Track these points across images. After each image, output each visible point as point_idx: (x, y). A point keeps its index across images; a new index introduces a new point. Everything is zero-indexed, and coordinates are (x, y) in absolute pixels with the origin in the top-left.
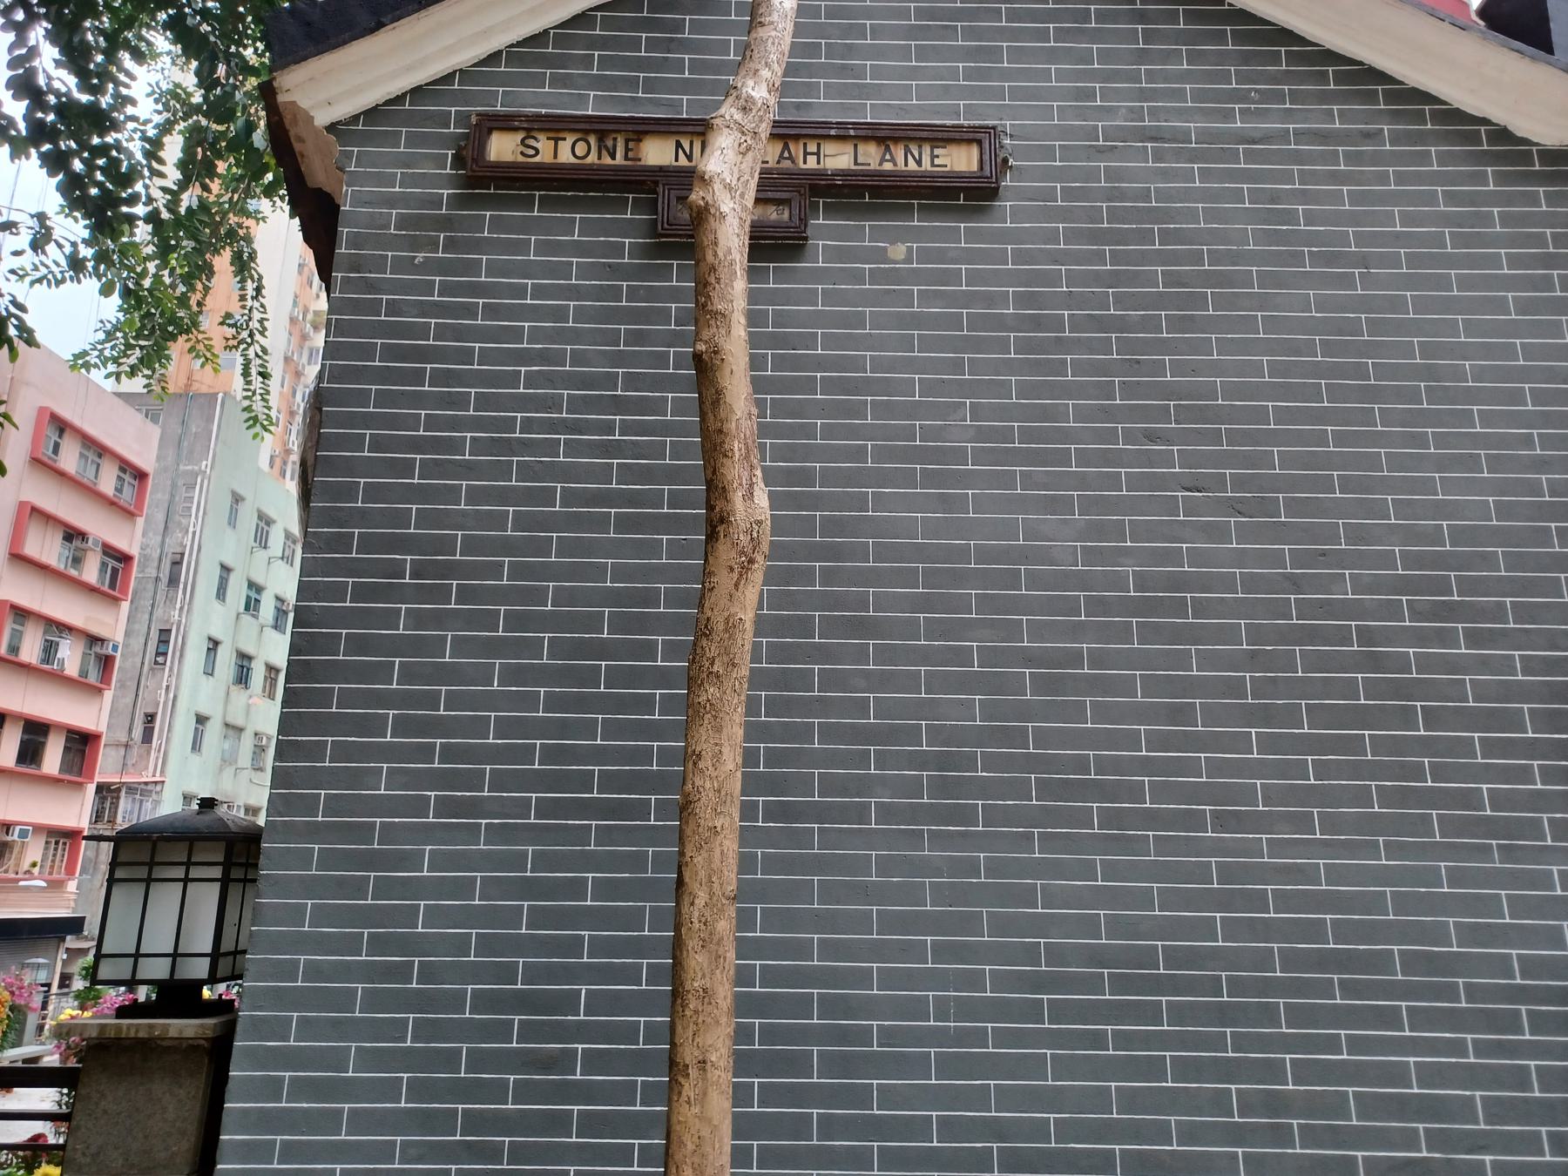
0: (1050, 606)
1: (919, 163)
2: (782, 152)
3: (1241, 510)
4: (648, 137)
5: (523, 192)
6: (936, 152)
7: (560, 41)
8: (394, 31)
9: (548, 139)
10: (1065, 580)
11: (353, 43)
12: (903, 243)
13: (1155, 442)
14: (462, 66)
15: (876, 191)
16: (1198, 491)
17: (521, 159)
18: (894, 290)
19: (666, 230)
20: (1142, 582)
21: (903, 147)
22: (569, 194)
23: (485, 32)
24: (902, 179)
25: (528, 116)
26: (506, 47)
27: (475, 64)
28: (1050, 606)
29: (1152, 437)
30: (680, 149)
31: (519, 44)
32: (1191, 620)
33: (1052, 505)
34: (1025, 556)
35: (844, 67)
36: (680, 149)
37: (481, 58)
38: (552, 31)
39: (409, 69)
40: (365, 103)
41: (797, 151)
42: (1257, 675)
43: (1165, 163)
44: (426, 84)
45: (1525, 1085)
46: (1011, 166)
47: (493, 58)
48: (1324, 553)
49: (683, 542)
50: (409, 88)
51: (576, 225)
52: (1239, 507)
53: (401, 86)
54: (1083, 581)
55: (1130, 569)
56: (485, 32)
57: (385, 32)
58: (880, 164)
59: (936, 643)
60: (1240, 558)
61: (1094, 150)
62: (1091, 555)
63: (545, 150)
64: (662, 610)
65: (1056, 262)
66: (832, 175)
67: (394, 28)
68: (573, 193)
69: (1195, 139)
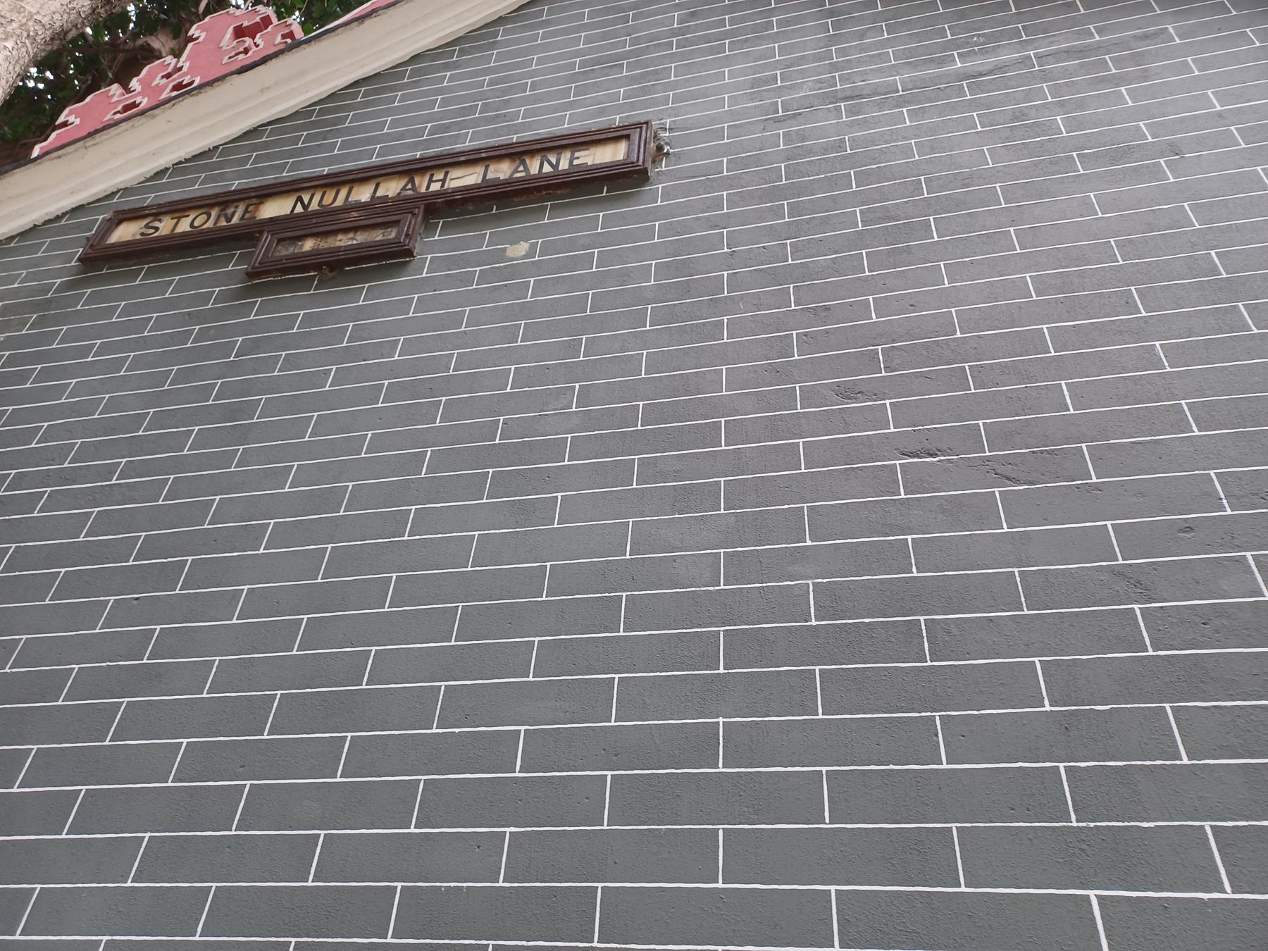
0: (663, 654)
2: (406, 185)
3: (1011, 475)
4: (269, 199)
6: (577, 155)
8: (59, 160)
9: (172, 219)
10: (697, 609)
11: (14, 171)
12: (526, 241)
13: (855, 398)
16: (931, 455)
18: (505, 285)
20: (831, 602)
21: (540, 158)
22: (178, 261)
23: (154, 154)
26: (173, 165)
28: (663, 654)
29: (847, 393)
30: (299, 203)
32: (929, 663)
33: (682, 499)
34: (630, 576)
35: (497, 116)
36: (299, 203)
42: (1083, 765)
43: (862, 115)
45: (1038, 57)
48: (1188, 528)
49: (135, 602)
50: (70, 208)
51: (172, 286)
52: (1007, 470)
54: (726, 609)
55: (810, 582)
56: (154, 154)
57: (49, 160)
59: (457, 730)
60: (1019, 548)
61: (772, 122)
62: (739, 567)
63: (165, 226)
64: (720, 885)
65: (716, 227)
66: (451, 193)
69: (902, 87)
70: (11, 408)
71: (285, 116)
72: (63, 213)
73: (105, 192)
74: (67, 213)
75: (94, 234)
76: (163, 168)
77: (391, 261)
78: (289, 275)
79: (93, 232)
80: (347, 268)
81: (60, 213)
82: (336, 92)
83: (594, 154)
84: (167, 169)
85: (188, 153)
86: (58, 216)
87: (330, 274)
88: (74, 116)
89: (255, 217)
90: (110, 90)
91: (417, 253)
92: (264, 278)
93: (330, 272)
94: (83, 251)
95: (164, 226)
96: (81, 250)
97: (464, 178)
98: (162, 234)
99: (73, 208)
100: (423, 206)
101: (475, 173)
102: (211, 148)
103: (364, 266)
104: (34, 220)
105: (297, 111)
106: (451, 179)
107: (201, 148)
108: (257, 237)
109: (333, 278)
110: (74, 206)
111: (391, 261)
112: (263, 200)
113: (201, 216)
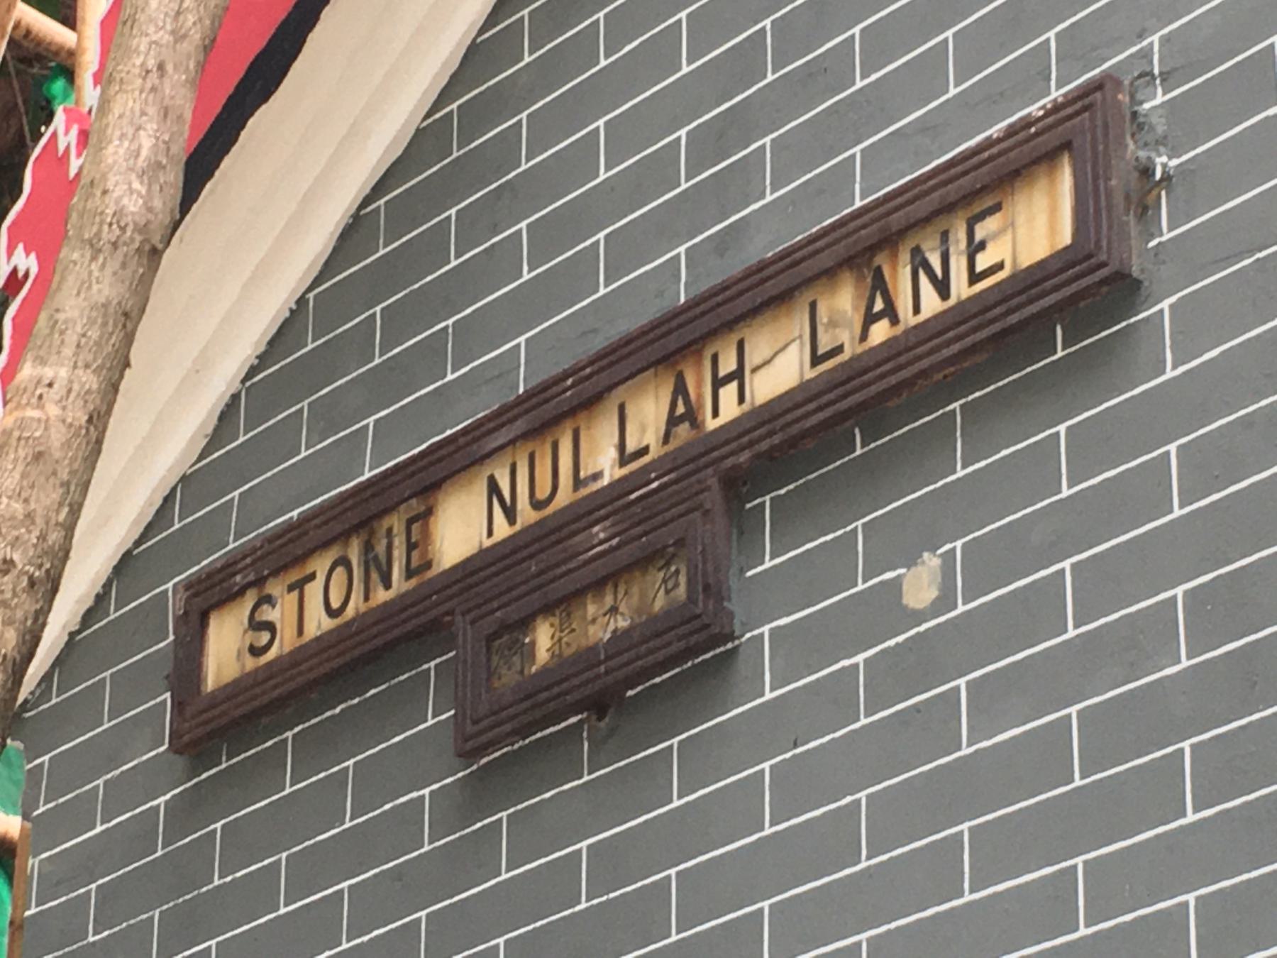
1: (943, 288)
4: (441, 496)
5: (402, 678)
7: (403, 215)
12: (933, 550)
14: (184, 468)
15: (374, 657)
17: (251, 663)
19: (471, 737)
22: (338, 710)
24: (500, 565)
25: (255, 550)
26: (243, 381)
27: (247, 374)
31: (264, 359)
37: (210, 430)
38: (311, 296)
39: (261, 274)
40: (331, 229)
41: (699, 384)
44: (138, 543)
46: (1167, 178)
47: (228, 415)
53: (92, 575)
56: (197, 371)
58: (864, 336)
67: (181, 241)
68: (343, 706)
70: (236, 493)
71: (399, 153)
72: (104, 586)
73: (151, 505)
74: (107, 586)
75: (175, 640)
76: (227, 398)
77: (700, 659)
78: (535, 733)
79: (171, 638)
80: (630, 693)
81: (98, 589)
82: (474, 40)
83: (1013, 224)
84: (235, 397)
85: (258, 343)
86: (98, 596)
87: (602, 724)
88: (30, 857)
89: (428, 565)
90: (54, 135)
91: (743, 624)
92: (497, 750)
93: (600, 719)
94: (172, 697)
95: (282, 614)
96: (168, 695)
97: (777, 361)
98: (287, 650)
99: (115, 568)
100: (713, 482)
101: (793, 340)
102: (294, 307)
103: (658, 680)
104: (64, 627)
105: (418, 130)
106: (754, 370)
107: (274, 319)
108: (449, 622)
109: (612, 731)
110: (115, 562)
111: (700, 659)
112: (431, 501)
113: (334, 575)
